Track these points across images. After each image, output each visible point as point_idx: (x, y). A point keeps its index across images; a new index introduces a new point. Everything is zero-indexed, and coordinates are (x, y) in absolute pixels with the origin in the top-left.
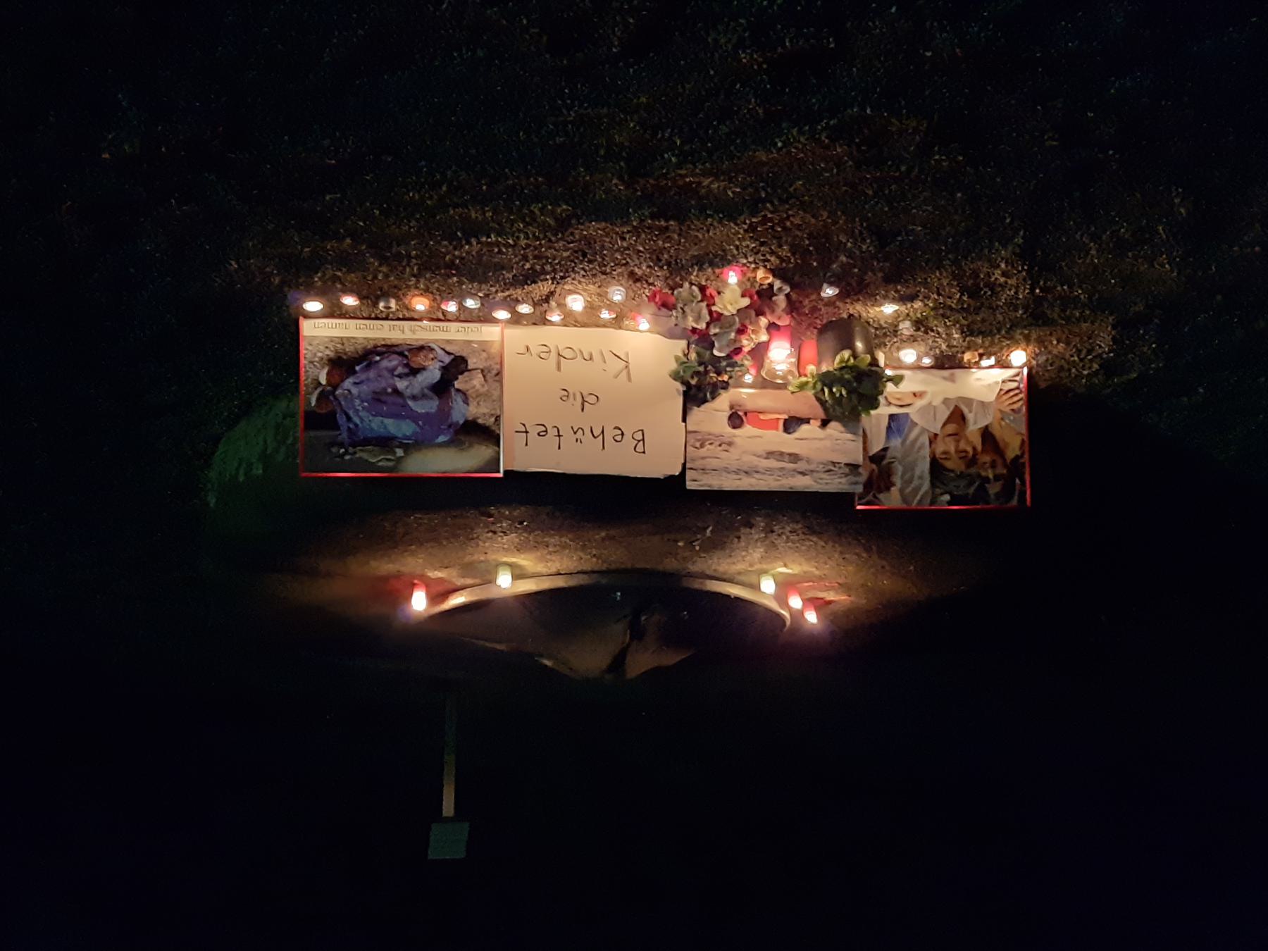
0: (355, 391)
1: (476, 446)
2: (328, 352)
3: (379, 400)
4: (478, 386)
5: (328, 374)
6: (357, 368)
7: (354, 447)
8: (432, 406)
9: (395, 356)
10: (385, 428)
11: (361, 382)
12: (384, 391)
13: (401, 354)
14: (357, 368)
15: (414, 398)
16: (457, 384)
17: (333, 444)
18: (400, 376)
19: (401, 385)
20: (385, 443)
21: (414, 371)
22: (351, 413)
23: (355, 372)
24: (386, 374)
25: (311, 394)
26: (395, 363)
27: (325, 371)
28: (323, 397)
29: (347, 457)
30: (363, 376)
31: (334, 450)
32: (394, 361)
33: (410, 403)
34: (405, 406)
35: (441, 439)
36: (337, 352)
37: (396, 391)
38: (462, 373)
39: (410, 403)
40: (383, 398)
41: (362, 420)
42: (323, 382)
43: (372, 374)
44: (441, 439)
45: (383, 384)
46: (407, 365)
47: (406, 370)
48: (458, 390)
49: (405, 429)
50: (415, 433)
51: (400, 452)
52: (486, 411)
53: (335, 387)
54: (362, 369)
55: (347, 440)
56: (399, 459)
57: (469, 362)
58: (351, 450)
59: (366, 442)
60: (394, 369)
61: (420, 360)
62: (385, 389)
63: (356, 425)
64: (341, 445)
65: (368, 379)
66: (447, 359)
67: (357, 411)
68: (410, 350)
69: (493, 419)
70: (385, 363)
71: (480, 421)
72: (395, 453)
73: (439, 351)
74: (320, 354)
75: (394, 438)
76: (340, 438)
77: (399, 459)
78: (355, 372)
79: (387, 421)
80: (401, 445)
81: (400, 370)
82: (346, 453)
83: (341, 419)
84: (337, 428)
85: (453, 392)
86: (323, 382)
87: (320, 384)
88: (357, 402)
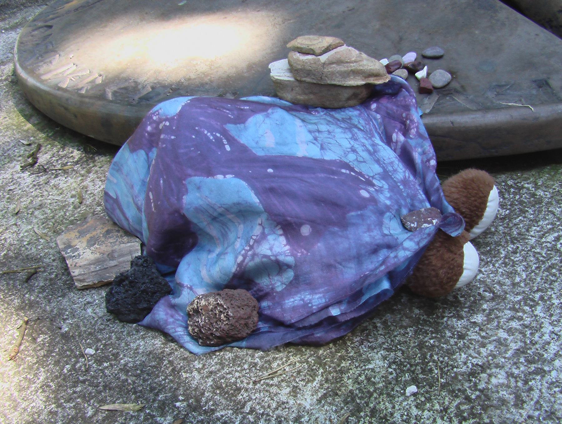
0: (392, 228)
1: (84, 85)
2: (459, 324)
3: (334, 205)
4: (81, 244)
5: (459, 269)
6: (386, 285)
7: (391, 84)
8: (204, 192)
9: (290, 317)
10: (315, 134)
11: (375, 250)
12: (320, 227)
13: (277, 323)
14: (386, 285)
15: (244, 213)
16: (132, 248)
17: (444, 91)
18: (279, 267)
19: (277, 246)
20: (316, 95)
21: (242, 280)
22: (401, 172)
23: (391, 275)
24: (317, 274)
25: (499, 219)
26: (292, 301)
27: (467, 275)
28: (472, 212)
29: (410, 58)
30: (369, 265)
31: (441, 77)
32: (298, 303)
33: (253, 199)
34: (266, 192)
35: (172, 107)
36: (438, 330)
37: (289, 227)
38: (121, 279)
39: (253, 199)
40: (315, 211)
41: (373, 153)
42: (469, 249)
43: (349, 274)
44: (172, 107)
45: (320, 246)
46: (261, 297)
47: (264, 282)
48: (130, 233)
49: (273, 133)
50: (241, 119)
51: (279, 70)
52: (61, 181)
53: (440, 236)
54: (377, 283)
55: (410, 97)
56: (281, 52)
57: (102, 311)
58: (401, 75)
59: (371, 94)
60: (295, 285)
61: (232, 310)
62: (317, 233)
63: (388, 140)
64: (425, 91)
65: (359, 259)
66: (161, 313)
67: (386, 176)
68: (255, 333)
69: (43, 159)
70: (317, 299)
71: (77, 154)
72: (292, 69)
73: (180, 332)
74: (479, 318)
75: (301, 107)
76: (429, 103)
77: (281, 52)
78: (391, 275)
79: (314, 152)
80: (276, 89)
81: (278, 283)
82: (412, 70)
83: (424, 152)
84: (437, 137)
85: (146, 233)
86: (469, 249)
87: (476, 242)
88: (175, 413)
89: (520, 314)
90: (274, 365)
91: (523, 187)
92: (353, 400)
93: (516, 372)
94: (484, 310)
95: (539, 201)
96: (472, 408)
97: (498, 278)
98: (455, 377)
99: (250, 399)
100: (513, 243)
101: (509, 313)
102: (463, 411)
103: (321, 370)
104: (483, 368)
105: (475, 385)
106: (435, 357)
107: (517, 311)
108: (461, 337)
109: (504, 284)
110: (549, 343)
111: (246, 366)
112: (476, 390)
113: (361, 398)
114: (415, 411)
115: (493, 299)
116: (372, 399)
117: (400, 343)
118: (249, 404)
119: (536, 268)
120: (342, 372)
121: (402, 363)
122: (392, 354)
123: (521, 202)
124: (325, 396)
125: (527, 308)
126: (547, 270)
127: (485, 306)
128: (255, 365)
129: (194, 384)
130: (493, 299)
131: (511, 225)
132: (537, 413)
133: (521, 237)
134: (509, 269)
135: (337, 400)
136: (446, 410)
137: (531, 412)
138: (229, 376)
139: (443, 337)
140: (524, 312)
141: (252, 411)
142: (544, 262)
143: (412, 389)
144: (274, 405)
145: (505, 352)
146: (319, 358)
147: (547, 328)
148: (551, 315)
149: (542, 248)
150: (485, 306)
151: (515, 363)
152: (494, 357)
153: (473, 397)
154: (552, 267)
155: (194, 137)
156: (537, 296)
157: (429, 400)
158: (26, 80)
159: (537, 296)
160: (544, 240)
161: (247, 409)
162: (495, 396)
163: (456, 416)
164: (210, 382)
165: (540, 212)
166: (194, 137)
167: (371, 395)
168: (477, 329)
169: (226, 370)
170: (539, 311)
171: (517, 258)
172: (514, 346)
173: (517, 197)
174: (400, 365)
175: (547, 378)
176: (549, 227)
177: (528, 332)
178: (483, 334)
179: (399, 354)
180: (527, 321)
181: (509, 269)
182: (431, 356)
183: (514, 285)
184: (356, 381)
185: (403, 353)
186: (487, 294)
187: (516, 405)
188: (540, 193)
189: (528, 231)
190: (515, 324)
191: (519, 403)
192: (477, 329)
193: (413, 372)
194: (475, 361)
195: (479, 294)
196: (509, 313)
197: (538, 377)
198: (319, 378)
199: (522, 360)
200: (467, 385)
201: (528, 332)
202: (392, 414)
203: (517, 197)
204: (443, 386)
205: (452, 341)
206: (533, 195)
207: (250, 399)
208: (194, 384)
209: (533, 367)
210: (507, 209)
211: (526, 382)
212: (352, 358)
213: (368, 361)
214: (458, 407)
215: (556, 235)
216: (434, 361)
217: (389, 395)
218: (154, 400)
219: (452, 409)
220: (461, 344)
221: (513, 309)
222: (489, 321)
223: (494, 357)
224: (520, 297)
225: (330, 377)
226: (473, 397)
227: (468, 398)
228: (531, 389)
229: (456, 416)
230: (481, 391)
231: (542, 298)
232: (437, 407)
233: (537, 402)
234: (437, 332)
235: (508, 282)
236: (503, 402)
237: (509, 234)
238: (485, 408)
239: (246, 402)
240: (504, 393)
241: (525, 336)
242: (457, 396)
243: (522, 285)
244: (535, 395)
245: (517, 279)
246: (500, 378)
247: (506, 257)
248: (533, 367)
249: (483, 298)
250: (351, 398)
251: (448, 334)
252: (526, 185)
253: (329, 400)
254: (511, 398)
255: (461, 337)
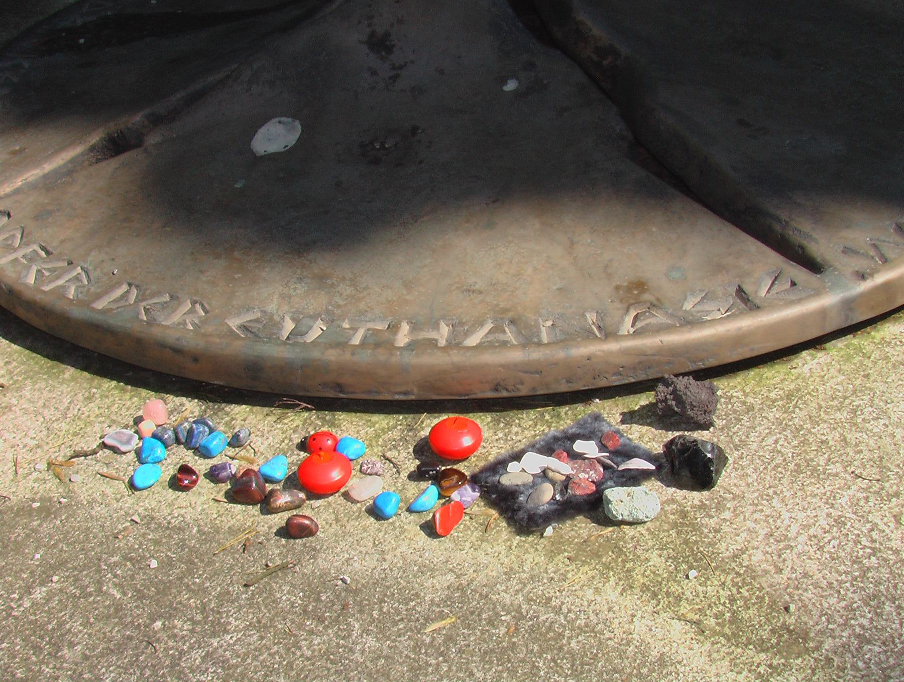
74: (727, 515)
89: (761, 507)
90: (569, 575)
91: (732, 396)
92: (648, 589)
93: (769, 550)
94: (729, 509)
95: (751, 408)
96: (744, 579)
97: (733, 481)
98: (723, 560)
99: (563, 603)
100: (738, 450)
101: (751, 508)
102: (738, 583)
103: (611, 573)
104: (743, 551)
105: (740, 563)
106: (701, 549)
107: (757, 505)
108: (717, 531)
109: (740, 486)
110: (790, 526)
111: (545, 581)
112: (742, 567)
113: (653, 587)
114: (700, 589)
115: (734, 499)
116: (663, 585)
117: (667, 543)
118: (564, 607)
119: (764, 469)
120: (629, 571)
121: (676, 558)
122: (665, 552)
123: (735, 412)
124: (624, 590)
125: (764, 502)
126: (774, 469)
127: (728, 506)
128: (552, 578)
129: (508, 602)
130: (734, 499)
131: (731, 434)
132: (794, 575)
133: (743, 444)
134: (740, 472)
135: (635, 591)
136: (724, 584)
137: (789, 576)
138: (535, 590)
139: (702, 533)
140: (762, 504)
141: (569, 611)
142: (769, 464)
143: (693, 574)
144: (586, 603)
145: (757, 537)
146: (604, 564)
147: (785, 515)
148: (786, 505)
149: (765, 452)
150: (728, 506)
151: (767, 544)
152: (749, 542)
153: (742, 572)
154: (777, 466)
155: (82, 41)
156: (771, 491)
157: (708, 579)
158: (740, 329)
159: (771, 491)
160: (764, 443)
161: (565, 609)
162: (758, 568)
163: (733, 586)
164: (520, 597)
165: (755, 418)
166: (82, 41)
167: (661, 583)
168: (728, 523)
169: (529, 587)
170: (775, 502)
171: (745, 462)
172: (762, 532)
173: (730, 406)
174: (675, 559)
175: (795, 550)
176: (767, 431)
177: (771, 520)
178: (735, 526)
179: (671, 551)
180: (768, 512)
181: (740, 472)
182: (698, 548)
183: (748, 485)
184: (643, 575)
185: (673, 550)
186: (727, 495)
187: (776, 573)
188: (750, 400)
189: (747, 437)
190: (757, 516)
191: (780, 571)
192: (728, 523)
193: (688, 562)
194: (734, 547)
195: (721, 496)
196: (751, 508)
197: (788, 551)
198: (612, 579)
199: (772, 541)
200: (734, 565)
201: (771, 520)
202: (683, 593)
203: (730, 406)
204: (716, 568)
205: (711, 535)
206: (744, 403)
207: (563, 603)
208: (508, 602)
209: (782, 545)
210: (723, 420)
211: (780, 556)
212: (632, 560)
213: (647, 560)
214: (732, 580)
215: (774, 438)
216: (701, 552)
217: (675, 581)
218: (480, 620)
219: (729, 582)
220: (718, 536)
221: (753, 504)
222: (737, 516)
223: (749, 542)
224: (756, 494)
225: (621, 576)
226: (742, 572)
227: (738, 574)
228: (784, 560)
229: (733, 586)
230: (747, 567)
231: (775, 493)
232: (716, 583)
233: (792, 568)
234: (695, 530)
235: (743, 483)
236: (766, 572)
237: (732, 442)
238: (754, 578)
239: (560, 607)
240: (764, 566)
241: (768, 523)
242: (728, 573)
243: (755, 484)
244: (789, 563)
245: (750, 480)
246: (757, 556)
247: (734, 463)
248: (782, 545)
249: (725, 499)
250: (645, 588)
251: (706, 531)
252: (735, 394)
253: (629, 592)
254: (772, 569)
255: (717, 531)
